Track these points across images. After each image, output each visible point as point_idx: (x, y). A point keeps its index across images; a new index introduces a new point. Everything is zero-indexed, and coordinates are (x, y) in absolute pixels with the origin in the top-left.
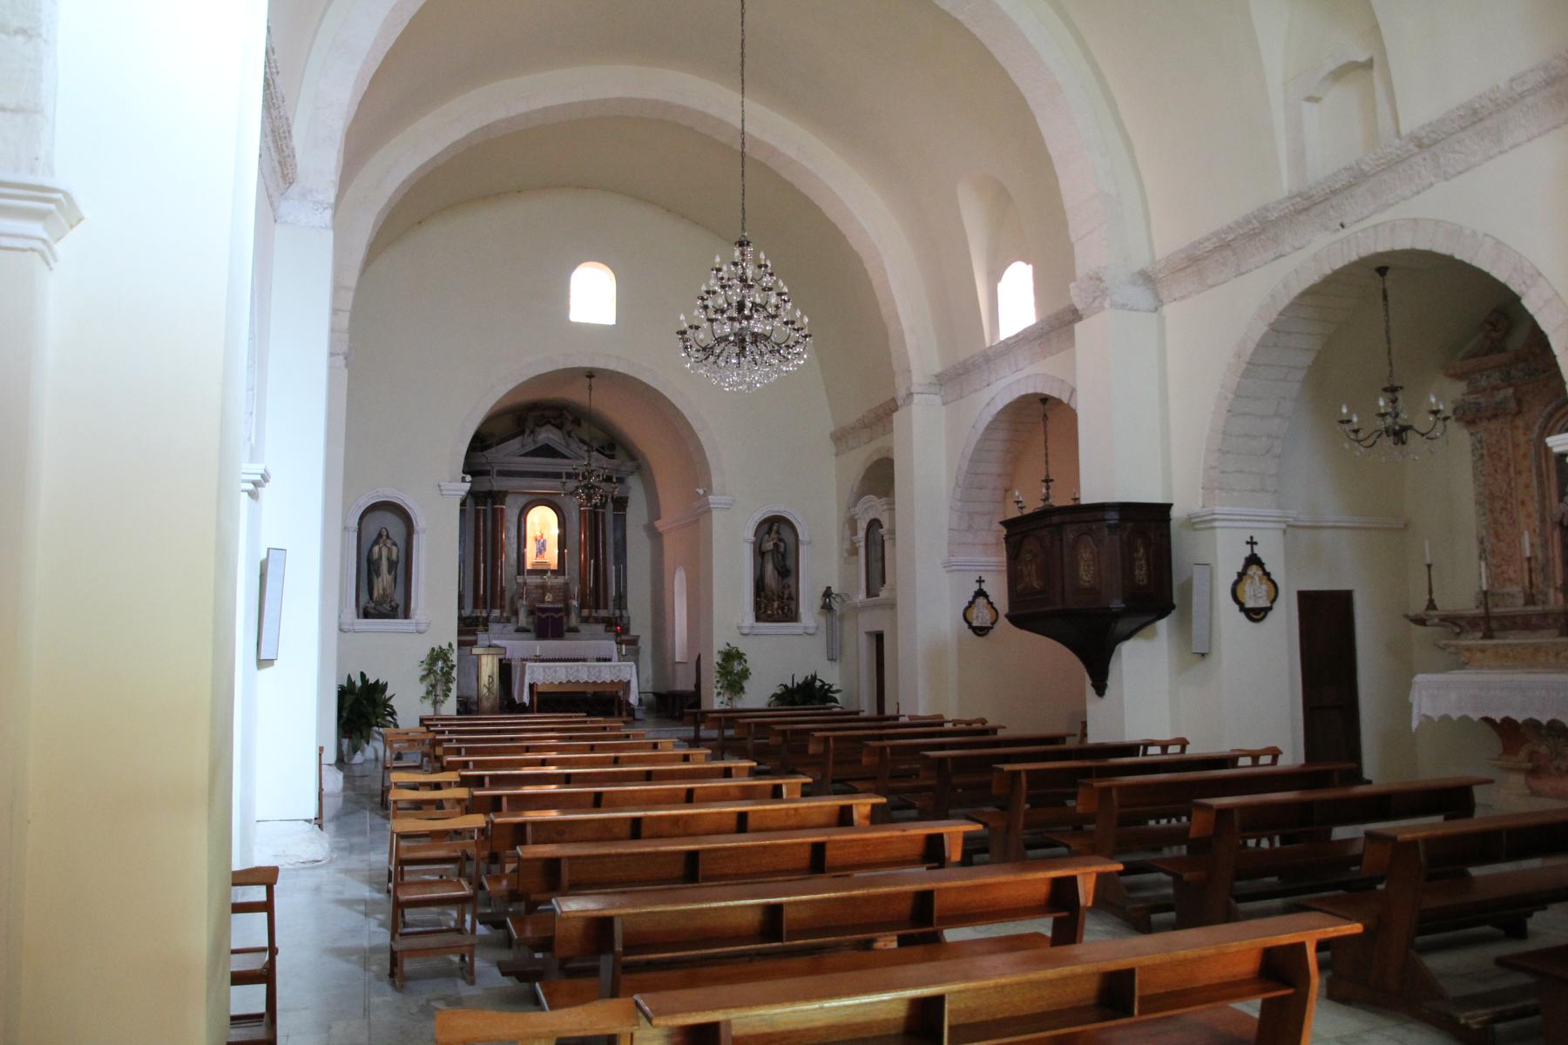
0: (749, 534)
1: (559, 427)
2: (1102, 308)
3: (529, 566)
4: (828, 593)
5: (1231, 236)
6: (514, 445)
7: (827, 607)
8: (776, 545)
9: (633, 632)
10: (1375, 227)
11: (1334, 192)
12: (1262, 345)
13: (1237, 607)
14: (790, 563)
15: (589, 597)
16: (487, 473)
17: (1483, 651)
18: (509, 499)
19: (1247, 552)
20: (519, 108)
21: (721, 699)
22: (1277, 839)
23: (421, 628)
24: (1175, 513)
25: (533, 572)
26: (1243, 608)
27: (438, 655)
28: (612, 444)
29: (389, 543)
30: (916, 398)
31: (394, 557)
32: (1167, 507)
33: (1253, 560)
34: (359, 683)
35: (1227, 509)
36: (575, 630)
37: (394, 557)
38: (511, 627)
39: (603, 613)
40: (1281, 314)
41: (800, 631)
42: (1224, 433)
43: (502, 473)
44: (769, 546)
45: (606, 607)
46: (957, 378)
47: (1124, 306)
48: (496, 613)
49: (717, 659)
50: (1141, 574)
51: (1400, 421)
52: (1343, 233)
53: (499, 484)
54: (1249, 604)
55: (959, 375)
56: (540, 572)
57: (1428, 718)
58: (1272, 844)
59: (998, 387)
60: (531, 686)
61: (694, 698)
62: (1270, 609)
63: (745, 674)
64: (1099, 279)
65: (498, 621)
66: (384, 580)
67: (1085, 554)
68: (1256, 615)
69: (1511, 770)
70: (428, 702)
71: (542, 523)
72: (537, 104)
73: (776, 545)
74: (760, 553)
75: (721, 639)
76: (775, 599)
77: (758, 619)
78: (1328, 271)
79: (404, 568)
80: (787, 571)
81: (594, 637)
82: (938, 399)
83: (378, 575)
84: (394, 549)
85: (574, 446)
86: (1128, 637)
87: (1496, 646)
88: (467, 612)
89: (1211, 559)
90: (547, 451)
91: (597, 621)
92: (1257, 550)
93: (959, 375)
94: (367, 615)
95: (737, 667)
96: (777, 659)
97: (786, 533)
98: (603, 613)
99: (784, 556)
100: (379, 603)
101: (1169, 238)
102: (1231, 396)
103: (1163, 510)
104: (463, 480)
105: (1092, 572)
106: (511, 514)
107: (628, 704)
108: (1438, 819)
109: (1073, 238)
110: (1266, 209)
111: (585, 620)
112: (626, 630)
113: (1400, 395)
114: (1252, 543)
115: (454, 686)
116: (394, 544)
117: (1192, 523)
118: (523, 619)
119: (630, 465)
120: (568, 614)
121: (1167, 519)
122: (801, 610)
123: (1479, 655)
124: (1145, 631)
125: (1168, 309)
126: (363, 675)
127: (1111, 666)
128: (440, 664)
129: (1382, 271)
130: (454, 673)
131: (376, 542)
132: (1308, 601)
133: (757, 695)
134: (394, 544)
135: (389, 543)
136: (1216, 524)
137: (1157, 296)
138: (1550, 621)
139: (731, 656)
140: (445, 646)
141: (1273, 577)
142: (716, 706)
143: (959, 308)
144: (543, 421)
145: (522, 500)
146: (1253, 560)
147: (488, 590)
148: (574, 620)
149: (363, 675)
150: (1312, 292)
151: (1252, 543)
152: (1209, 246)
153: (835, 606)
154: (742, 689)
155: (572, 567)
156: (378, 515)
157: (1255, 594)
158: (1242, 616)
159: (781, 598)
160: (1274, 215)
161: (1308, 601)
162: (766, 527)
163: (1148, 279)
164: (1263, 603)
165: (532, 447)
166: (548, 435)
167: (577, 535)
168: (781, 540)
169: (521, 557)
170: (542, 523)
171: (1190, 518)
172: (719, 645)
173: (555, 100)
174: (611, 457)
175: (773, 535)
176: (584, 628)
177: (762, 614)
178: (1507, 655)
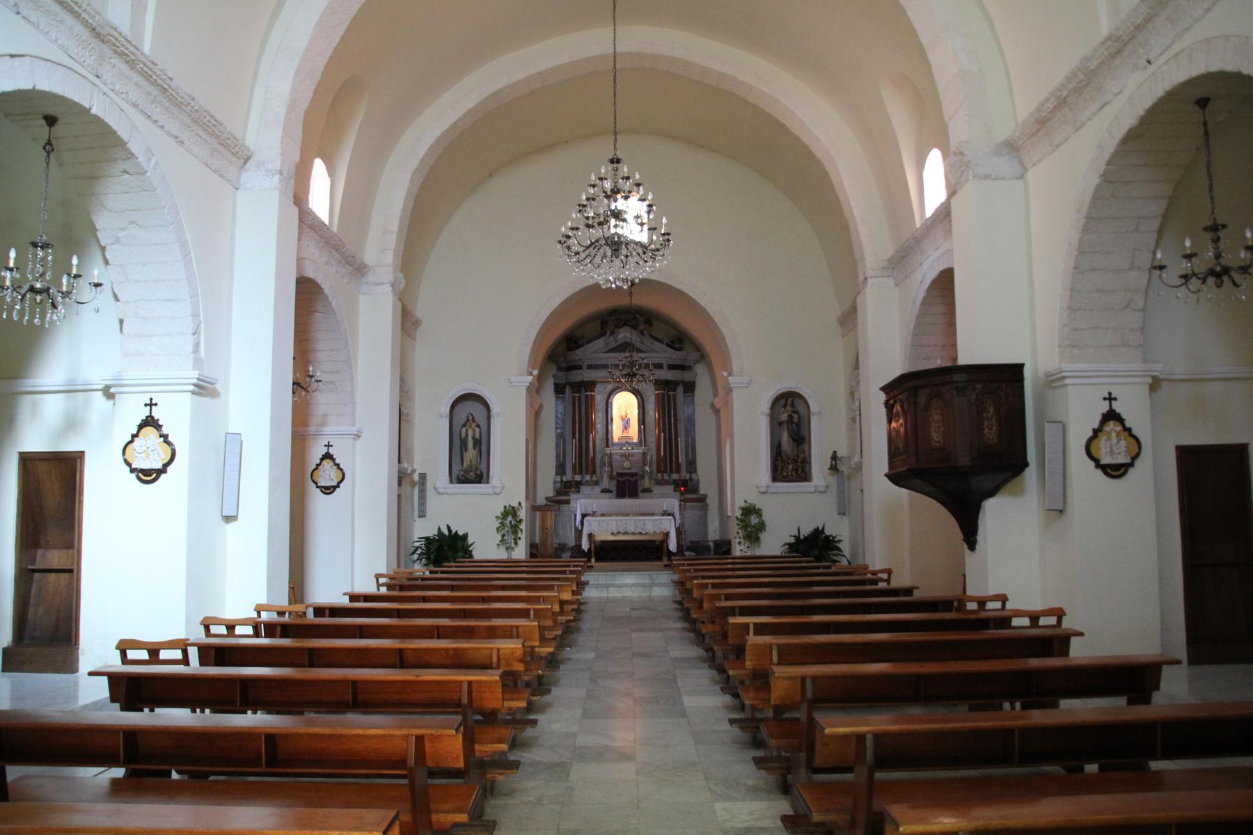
0: (766, 407)
1: (634, 327)
2: (967, 180)
3: (616, 440)
4: (834, 457)
5: (1064, 94)
6: (599, 343)
7: (834, 469)
8: (790, 416)
9: (702, 492)
10: (1176, 56)
11: (1138, 28)
12: (1097, 197)
13: (1092, 464)
14: (804, 432)
15: (671, 459)
16: (580, 367)
18: (599, 388)
19: (1105, 407)
20: (517, 76)
21: (742, 547)
22: (1018, 705)
23: (498, 490)
24: (1027, 373)
25: (621, 445)
26: (1098, 465)
27: (510, 512)
28: (679, 340)
29: (474, 425)
30: (870, 281)
31: (477, 436)
32: (1019, 368)
33: (1111, 416)
34: (446, 532)
35: (1079, 366)
36: (648, 490)
37: (477, 436)
38: (598, 489)
39: (675, 476)
40: (1109, 163)
41: (812, 490)
42: (1072, 290)
43: (590, 367)
44: (784, 417)
45: (678, 471)
46: (900, 261)
47: (987, 177)
48: (588, 478)
49: (738, 513)
50: (990, 432)
51: (1223, 262)
52: (1151, 69)
53: (586, 375)
54: (1106, 460)
55: (903, 257)
56: (626, 442)
58: (1013, 708)
59: (927, 263)
60: (590, 536)
61: (723, 547)
62: (1131, 465)
63: (762, 527)
64: (961, 153)
65: (587, 483)
66: (471, 454)
67: (936, 416)
68: (1115, 471)
70: (503, 548)
71: (625, 405)
72: (532, 71)
73: (790, 416)
74: (775, 424)
75: (737, 499)
76: (789, 463)
77: (774, 479)
78: (1141, 112)
79: (483, 444)
80: (800, 438)
81: (663, 496)
82: (890, 281)
83: (466, 450)
84: (477, 430)
85: (647, 340)
86: (992, 493)
88: (568, 477)
89: (1066, 417)
90: (624, 347)
91: (667, 483)
92: (1115, 405)
93: (903, 257)
94: (460, 481)
95: (754, 520)
96: (789, 514)
97: (801, 408)
98: (675, 476)
99: (798, 425)
100: (467, 472)
101: (1025, 105)
102: (1075, 253)
103: (1015, 371)
104: (531, 374)
105: (965, 432)
106: (599, 398)
107: (668, 550)
108: (1122, 701)
109: (946, 120)
110: (1087, 59)
111: (659, 483)
112: (695, 490)
113: (1221, 234)
114: (1110, 398)
115: (522, 535)
116: (478, 426)
117: (1053, 381)
118: (605, 483)
119: (694, 355)
120: (643, 477)
121: (1020, 379)
122: (813, 471)
124: (1008, 487)
125: (1030, 175)
126: (449, 527)
127: (980, 522)
128: (510, 518)
129: (1203, 103)
130: (523, 526)
131: (464, 425)
132: (1189, 458)
133: (773, 544)
134: (478, 426)
135: (474, 425)
136: (1067, 381)
137: (1021, 163)
139: (749, 511)
140: (516, 505)
141: (1134, 432)
142: (738, 554)
143: (896, 195)
144: (620, 324)
145: (610, 387)
146: (1111, 416)
147: (580, 457)
148: (646, 483)
149: (449, 527)
150: (1132, 137)
151: (1110, 398)
152: (1050, 105)
153: (841, 467)
154: (758, 539)
155: (652, 440)
156: (459, 406)
157: (1113, 449)
158: (1099, 472)
159: (795, 461)
160: (1093, 64)
161: (1189, 458)
162: (783, 401)
163: (1012, 147)
164: (1122, 459)
165: (613, 345)
166: (625, 334)
167: (652, 414)
168: (797, 413)
169: (608, 432)
170: (625, 405)
171: (1048, 375)
172: (740, 503)
173: (544, 65)
174: (680, 349)
175: (789, 408)
176: (657, 490)
177: (778, 473)
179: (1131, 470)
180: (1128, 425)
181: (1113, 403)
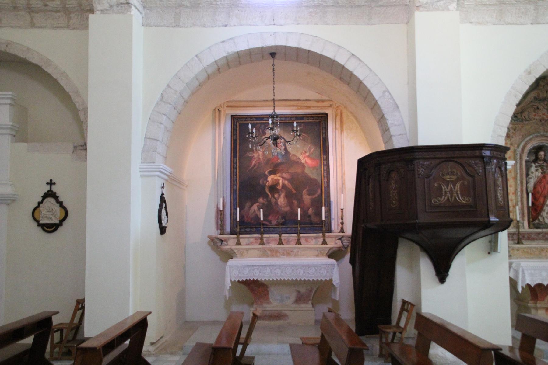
17: (518, 250)
19: (47, 188)
26: (39, 225)
33: (50, 194)
57: (528, 285)
69: (543, 308)
87: (525, 248)
123: (516, 252)
138: (541, 236)
146: (50, 194)
158: (40, 228)
178: (527, 252)
179: (60, 228)
180: (60, 200)
181: (53, 187)
